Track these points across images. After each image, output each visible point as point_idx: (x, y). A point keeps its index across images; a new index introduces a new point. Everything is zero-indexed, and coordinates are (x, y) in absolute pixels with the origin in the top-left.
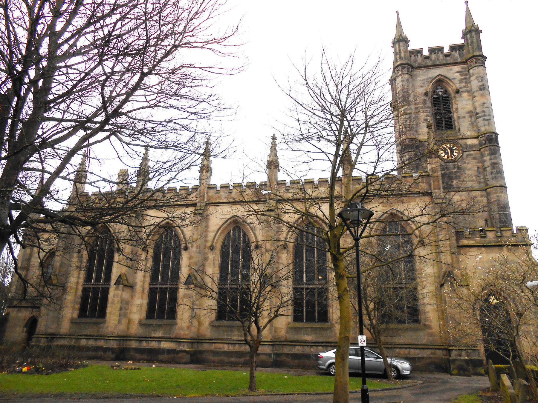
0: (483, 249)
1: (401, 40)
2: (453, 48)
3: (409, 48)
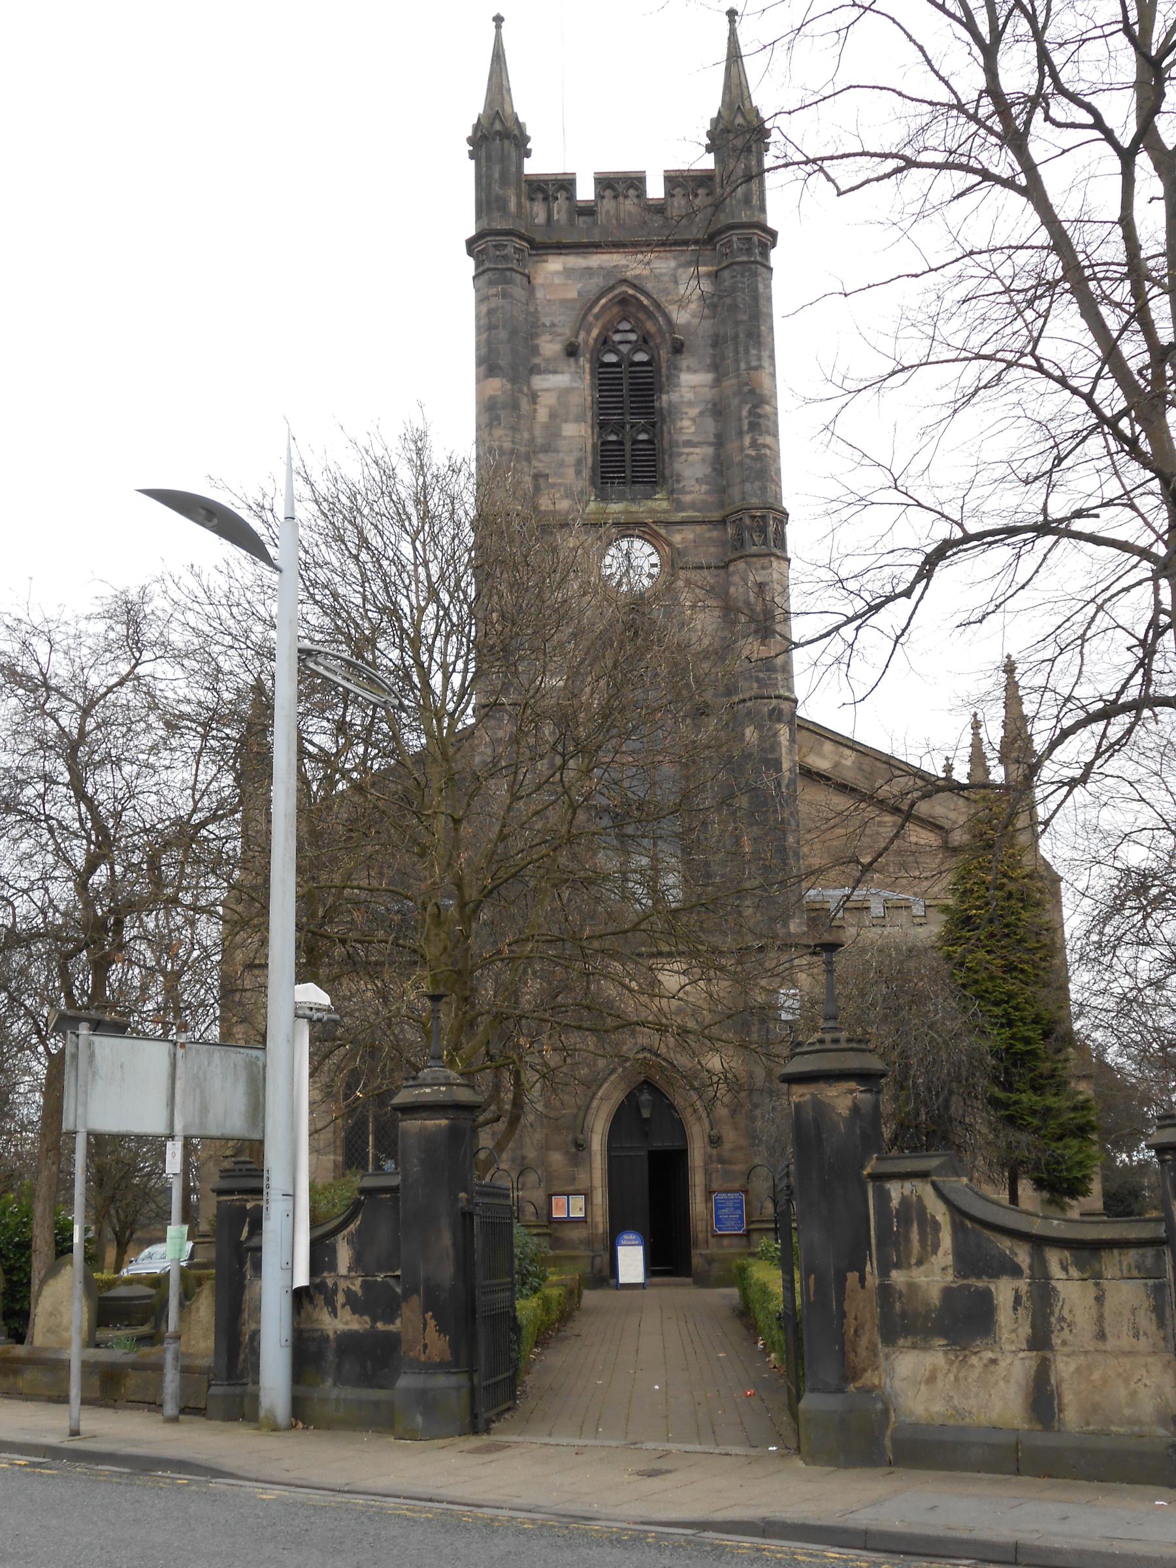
0: (81, 1468)
1: (497, 139)
2: (673, 180)
3: (531, 167)
